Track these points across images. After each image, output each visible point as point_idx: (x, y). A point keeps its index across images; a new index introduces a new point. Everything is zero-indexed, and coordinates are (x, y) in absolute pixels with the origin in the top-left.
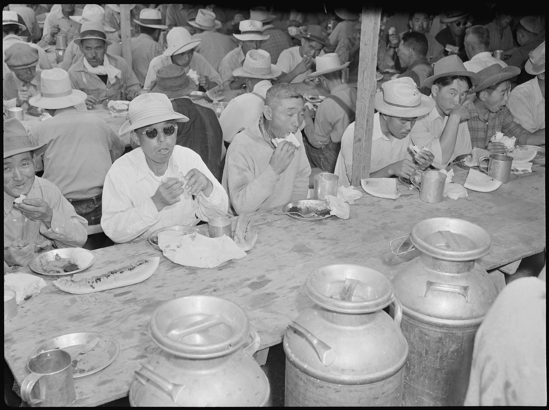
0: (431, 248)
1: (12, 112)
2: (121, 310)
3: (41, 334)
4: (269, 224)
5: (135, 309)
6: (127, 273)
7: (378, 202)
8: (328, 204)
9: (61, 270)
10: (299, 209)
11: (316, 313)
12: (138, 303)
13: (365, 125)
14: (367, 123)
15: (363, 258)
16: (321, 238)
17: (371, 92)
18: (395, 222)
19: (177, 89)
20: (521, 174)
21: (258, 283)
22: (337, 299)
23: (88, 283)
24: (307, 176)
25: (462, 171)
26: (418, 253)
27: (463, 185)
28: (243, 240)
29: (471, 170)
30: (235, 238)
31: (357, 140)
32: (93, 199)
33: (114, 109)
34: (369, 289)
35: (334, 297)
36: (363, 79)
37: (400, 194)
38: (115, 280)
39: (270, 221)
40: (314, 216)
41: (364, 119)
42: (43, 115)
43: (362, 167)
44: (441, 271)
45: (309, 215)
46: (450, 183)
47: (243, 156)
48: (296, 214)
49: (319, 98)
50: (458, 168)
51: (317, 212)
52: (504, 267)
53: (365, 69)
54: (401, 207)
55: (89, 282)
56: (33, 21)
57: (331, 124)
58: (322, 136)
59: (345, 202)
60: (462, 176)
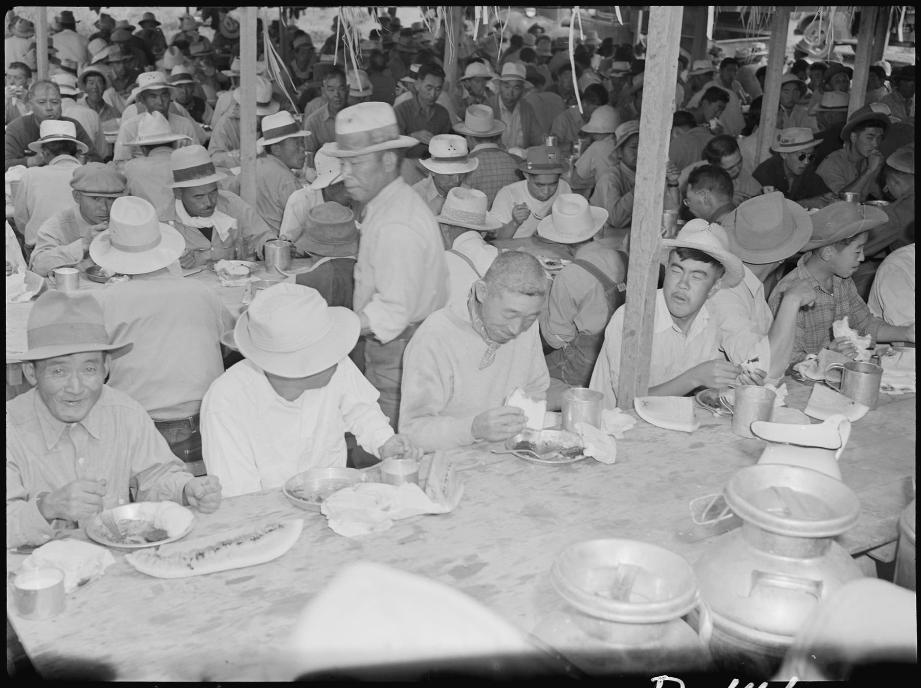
0: (759, 513)
1: (60, 274)
2: (237, 608)
3: (104, 644)
4: (482, 469)
5: (261, 607)
6: (248, 545)
7: (662, 436)
8: (581, 438)
9: (141, 539)
10: (532, 445)
11: (568, 621)
12: (266, 596)
13: (642, 309)
14: (645, 305)
15: (639, 529)
16: (569, 495)
17: (652, 254)
18: (692, 471)
19: (342, 242)
20: (898, 395)
21: (466, 568)
22: (605, 598)
23: (182, 561)
24: (543, 390)
25: (799, 389)
26: (738, 522)
27: (803, 411)
28: (440, 496)
29: (817, 387)
30: (428, 490)
31: (629, 333)
32: (188, 420)
33: (226, 274)
34: (659, 583)
35: (600, 593)
36: (640, 234)
37: (699, 424)
38: (228, 556)
39: (484, 464)
40: (556, 456)
41: (641, 298)
42: (111, 281)
43: (636, 378)
44: (775, 553)
45: (548, 456)
46: (782, 406)
47: (432, 352)
48: (528, 454)
49: (561, 263)
50: (793, 381)
51: (561, 450)
52: (877, 550)
53: (643, 218)
54: (700, 445)
55: (185, 559)
56: (96, 131)
57: (576, 304)
58: (562, 325)
59: (609, 435)
60: (801, 397)
